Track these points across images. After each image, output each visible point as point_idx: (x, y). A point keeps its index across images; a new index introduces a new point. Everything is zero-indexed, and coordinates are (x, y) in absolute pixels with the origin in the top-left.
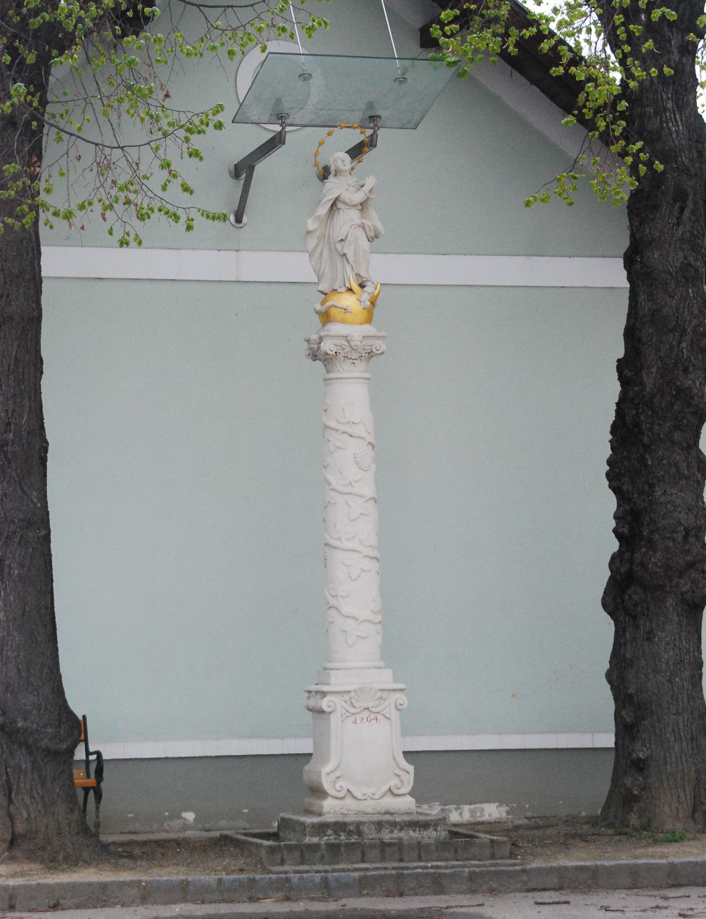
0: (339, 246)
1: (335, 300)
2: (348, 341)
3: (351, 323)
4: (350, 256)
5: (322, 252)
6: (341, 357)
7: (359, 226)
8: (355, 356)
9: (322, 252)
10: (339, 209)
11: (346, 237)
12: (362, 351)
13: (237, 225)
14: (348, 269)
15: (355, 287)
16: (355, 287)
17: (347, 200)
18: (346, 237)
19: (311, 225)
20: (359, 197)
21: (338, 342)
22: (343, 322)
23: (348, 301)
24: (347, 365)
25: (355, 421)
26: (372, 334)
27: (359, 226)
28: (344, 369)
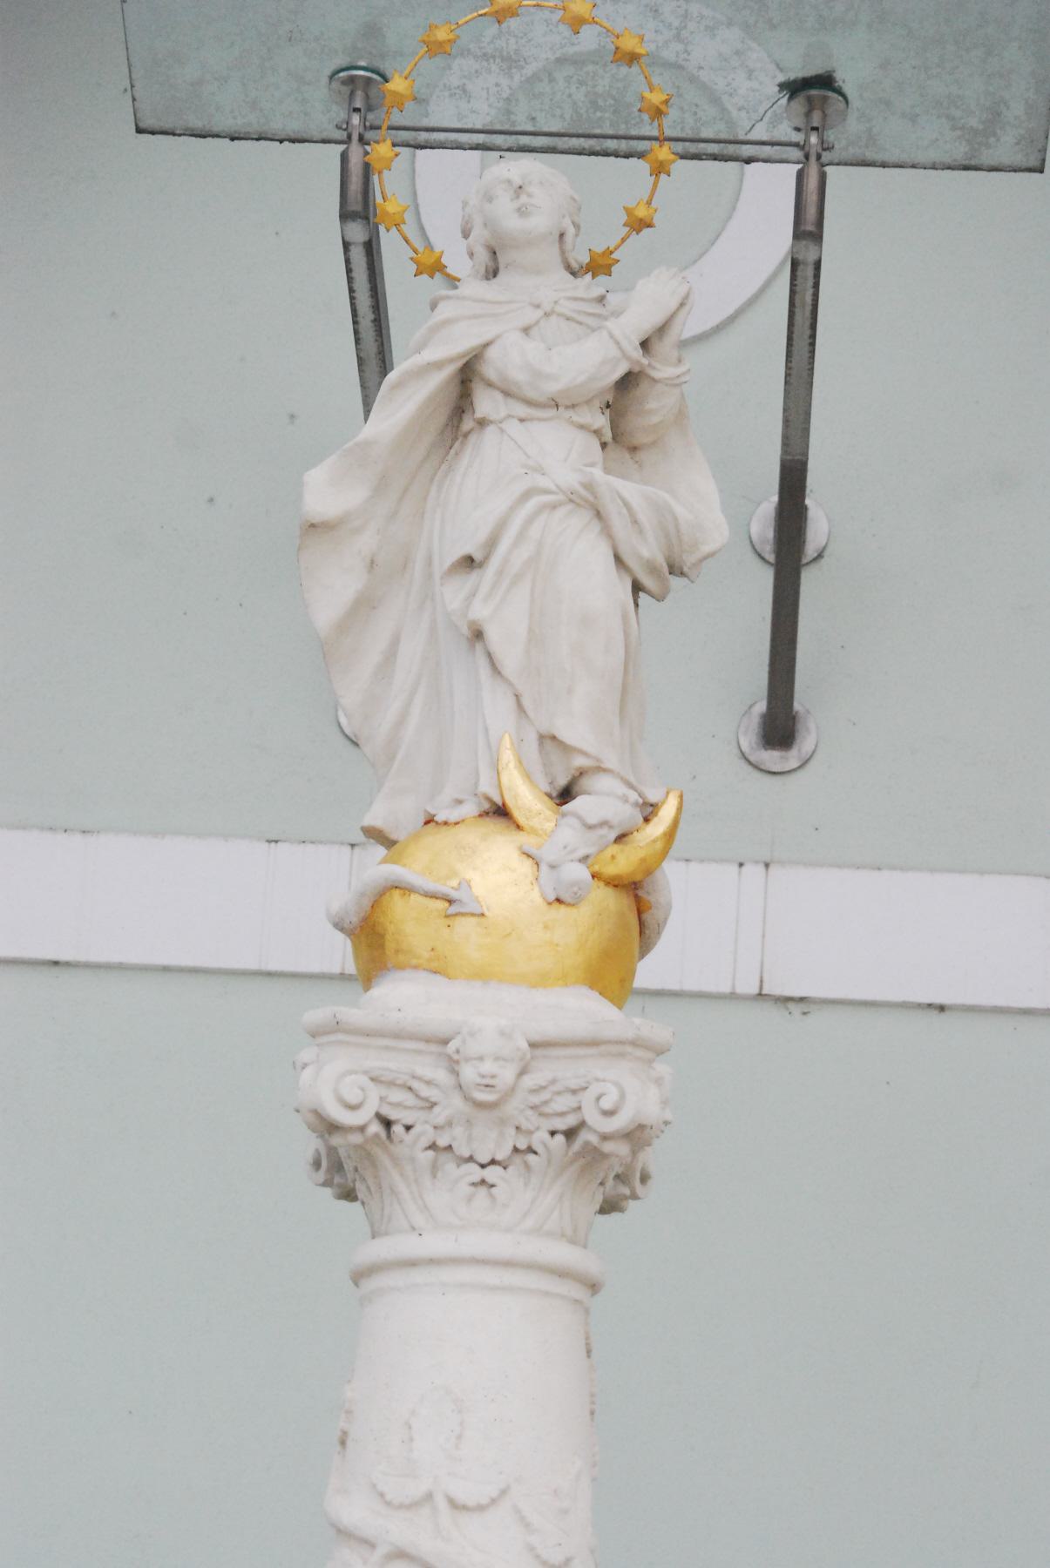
0: (453, 594)
1: (419, 865)
2: (453, 1066)
3: (482, 975)
4: (506, 639)
5: (395, 642)
6: (412, 1147)
7: (572, 499)
8: (490, 1143)
9: (395, 642)
10: (482, 423)
11: (491, 543)
12: (529, 1120)
13: (772, 758)
14: (497, 708)
15: (527, 798)
16: (527, 798)
17: (519, 376)
18: (491, 543)
19: (324, 492)
20: (589, 359)
21: (396, 1063)
22: (439, 968)
23: (495, 873)
24: (448, 1193)
25: (464, 1494)
26: (580, 1028)
27: (572, 499)
28: (438, 1215)
